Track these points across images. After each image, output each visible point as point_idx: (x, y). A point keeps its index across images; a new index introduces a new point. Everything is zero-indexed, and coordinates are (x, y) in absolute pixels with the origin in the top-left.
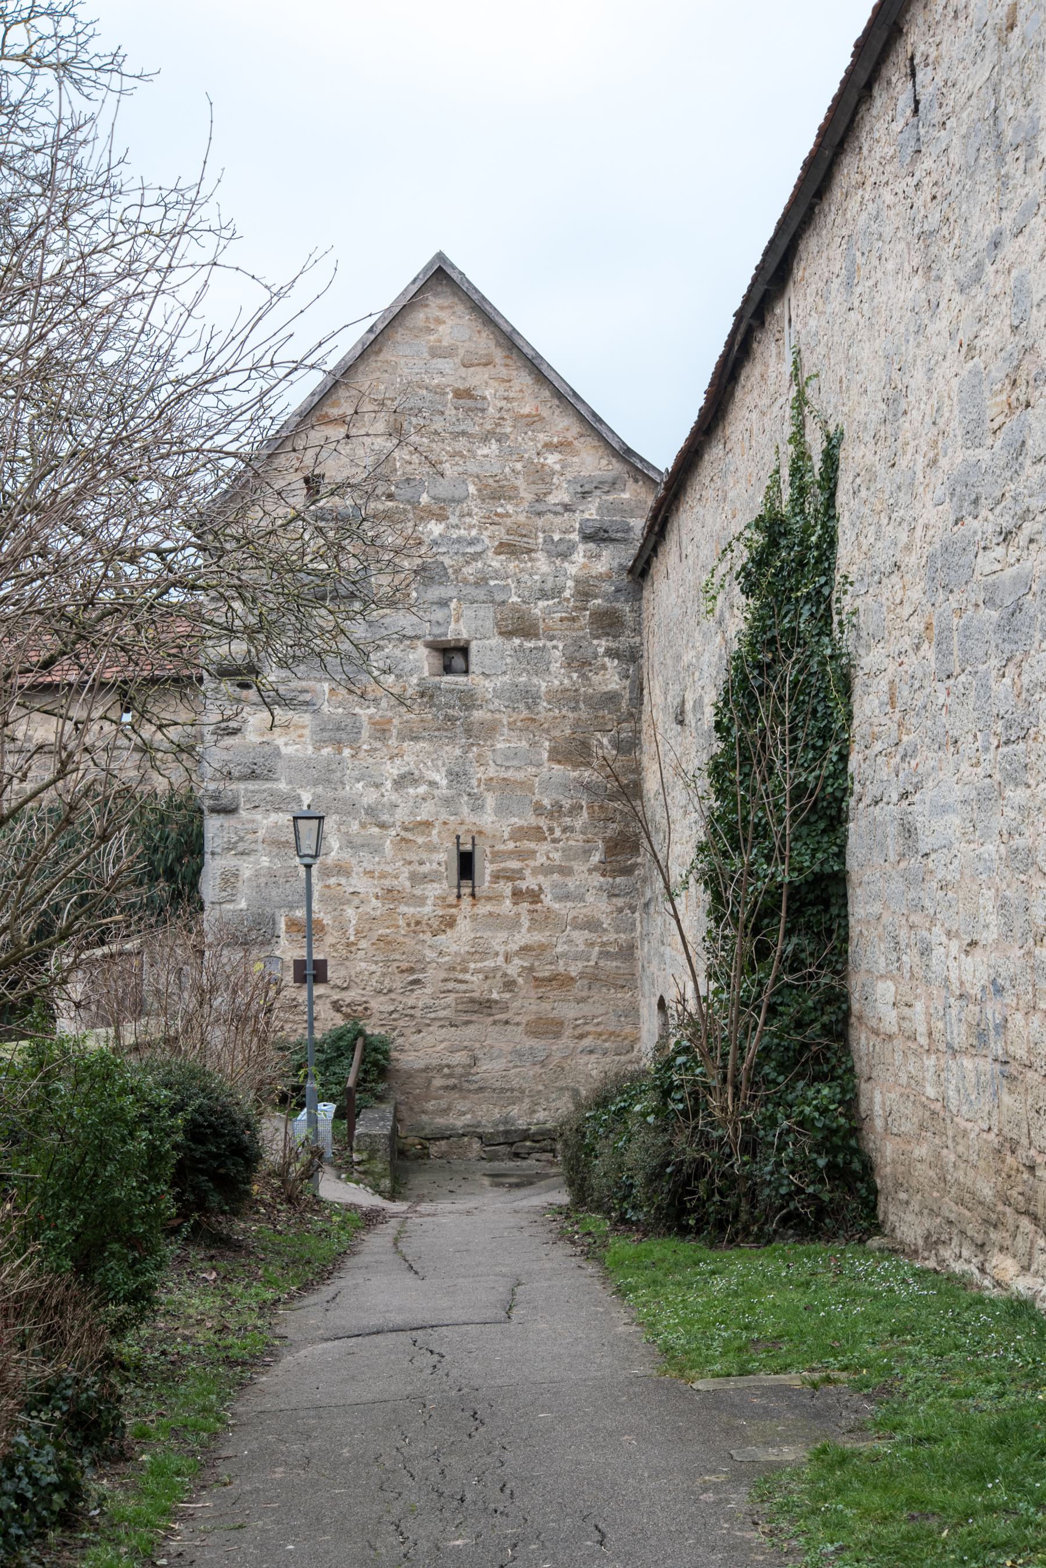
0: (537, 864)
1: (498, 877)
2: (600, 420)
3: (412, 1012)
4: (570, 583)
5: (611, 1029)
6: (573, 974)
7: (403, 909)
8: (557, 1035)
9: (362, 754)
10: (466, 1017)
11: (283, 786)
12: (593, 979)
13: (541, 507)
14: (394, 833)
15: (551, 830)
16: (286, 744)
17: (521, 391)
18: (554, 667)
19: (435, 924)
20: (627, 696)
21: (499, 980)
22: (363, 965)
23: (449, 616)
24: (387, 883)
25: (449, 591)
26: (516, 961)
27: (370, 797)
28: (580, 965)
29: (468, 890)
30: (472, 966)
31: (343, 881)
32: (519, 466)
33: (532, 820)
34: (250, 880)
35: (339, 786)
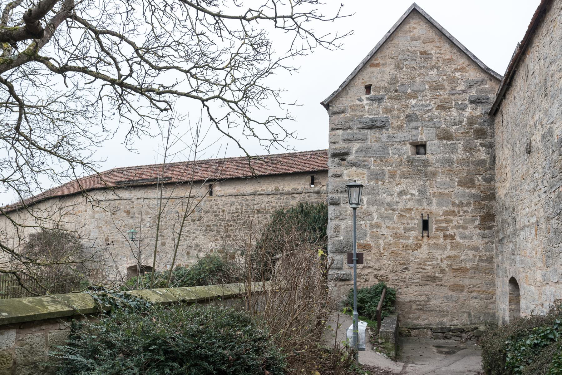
0: (454, 225)
1: (438, 230)
2: (477, 58)
3: (405, 280)
4: (465, 119)
5: (484, 289)
6: (468, 268)
7: (401, 241)
8: (462, 291)
9: (386, 184)
12: (476, 270)
13: (453, 92)
15: (459, 212)
18: (459, 151)
19: (413, 247)
20: (489, 161)
21: (438, 269)
22: (386, 261)
23: (419, 133)
24: (395, 231)
25: (419, 124)
26: (445, 262)
27: (389, 199)
28: (471, 264)
29: (426, 234)
30: (428, 263)
31: (378, 230)
32: (445, 77)
33: (451, 208)
34: (344, 229)
35: (377, 195)
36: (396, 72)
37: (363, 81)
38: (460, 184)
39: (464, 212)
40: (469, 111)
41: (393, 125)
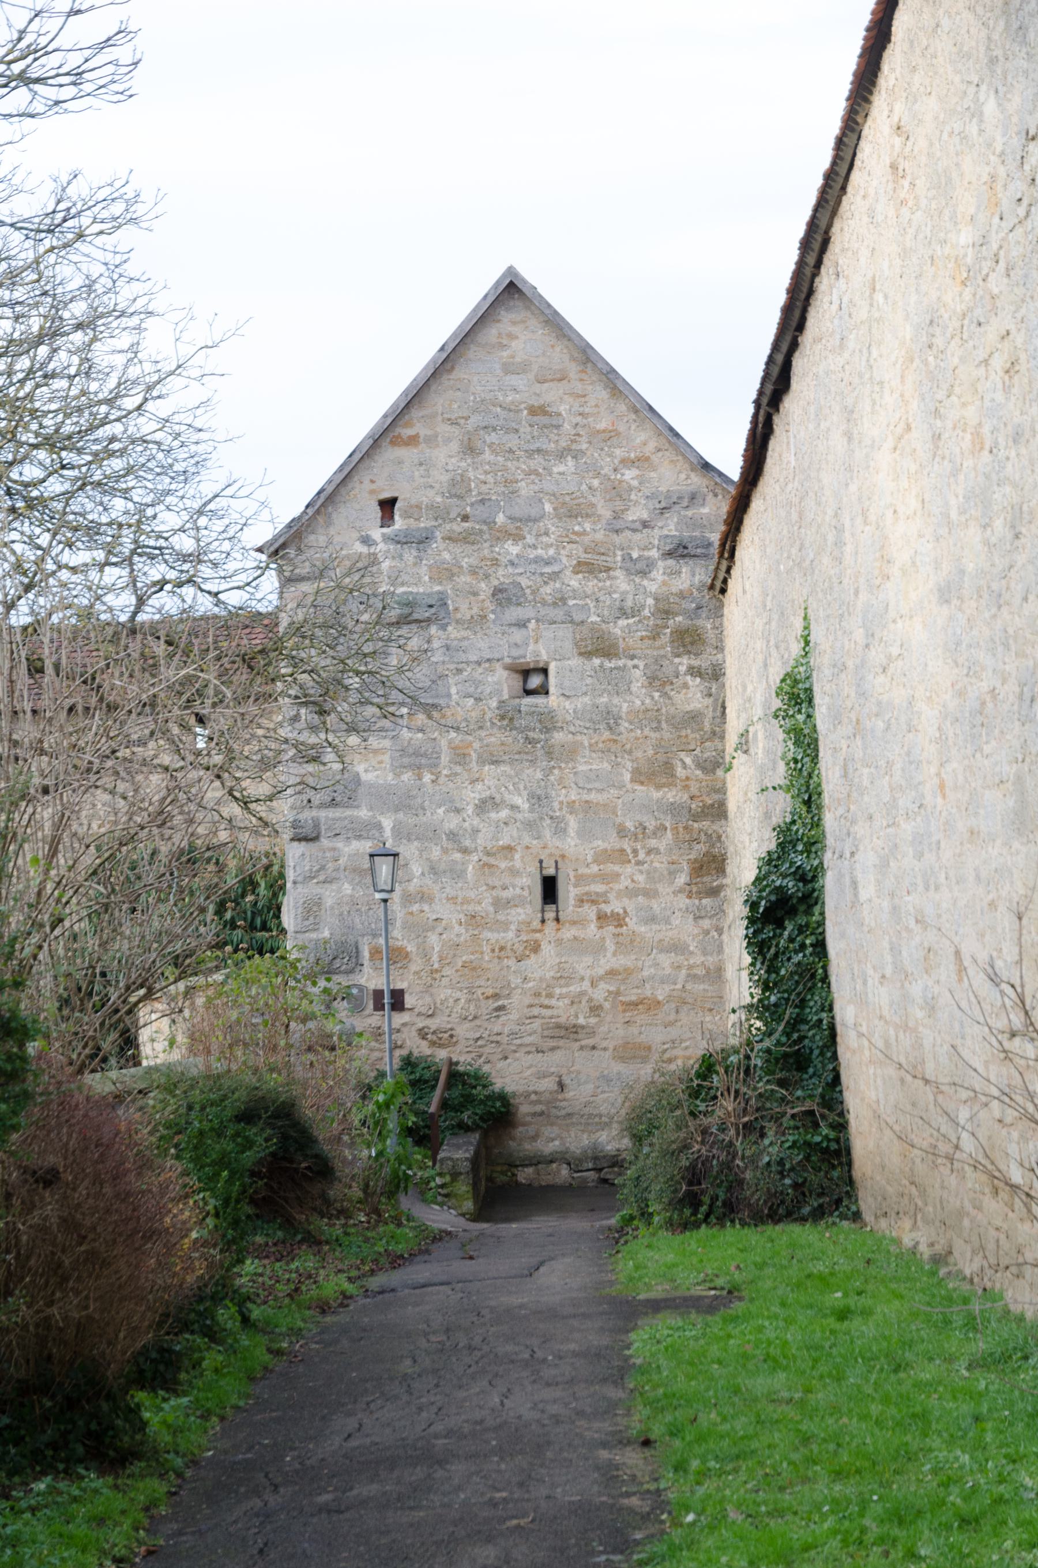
0: (622, 887)
3: (498, 1038)
4: (650, 601)
6: (660, 998)
9: (442, 780)
10: (552, 1043)
11: (363, 813)
12: (681, 1002)
14: (476, 858)
15: (635, 852)
16: (366, 771)
17: (596, 406)
18: (635, 687)
20: (711, 715)
24: (471, 908)
26: (602, 985)
27: (452, 823)
28: (667, 988)
29: (552, 915)
30: (558, 991)
31: (426, 908)
32: (596, 483)
34: (332, 908)
36: (463, 464)
37: (373, 486)
38: (640, 776)
39: (649, 852)
40: (656, 582)
41: (459, 616)
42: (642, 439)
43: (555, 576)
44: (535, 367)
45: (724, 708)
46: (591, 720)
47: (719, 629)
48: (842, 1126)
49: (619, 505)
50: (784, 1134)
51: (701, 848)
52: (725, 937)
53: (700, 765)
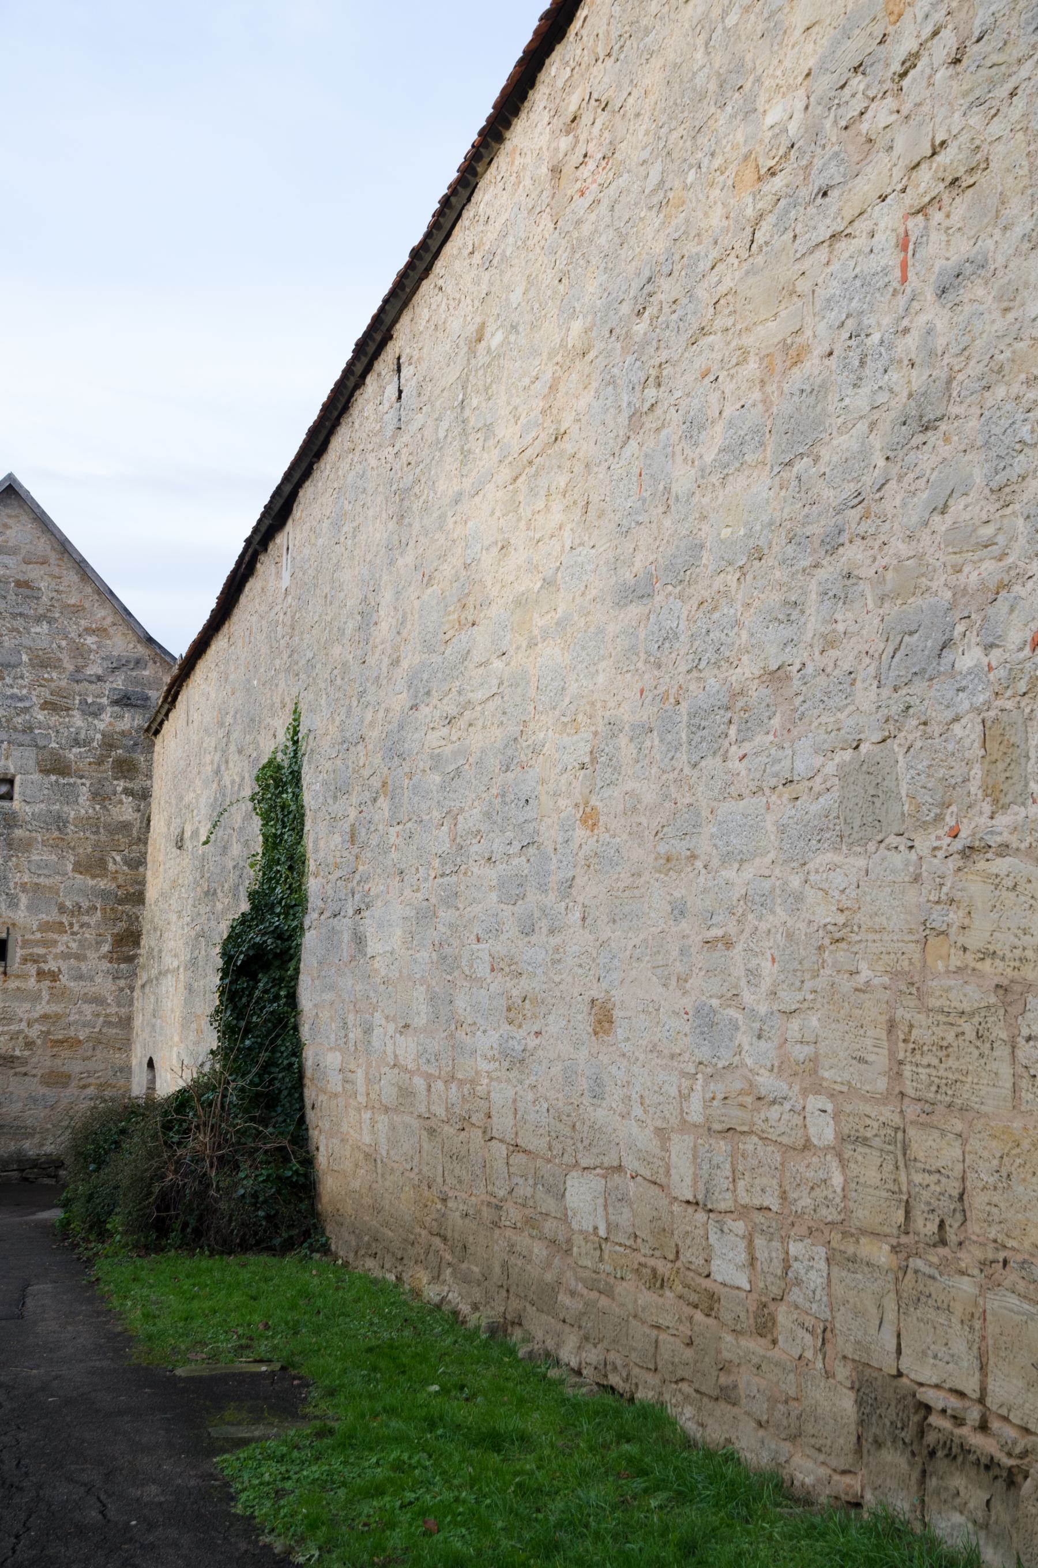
4: (99, 736)
12: (97, 1041)
15: (71, 925)
26: (36, 1026)
32: (64, 643)
38: (78, 867)
39: (82, 926)
40: (104, 722)
42: (102, 614)
43: (26, 710)
44: (23, 552)
45: (149, 821)
46: (45, 822)
47: (150, 762)
48: (309, 1162)
49: (80, 662)
50: (257, 1168)
51: (123, 925)
52: (135, 994)
53: (127, 862)
